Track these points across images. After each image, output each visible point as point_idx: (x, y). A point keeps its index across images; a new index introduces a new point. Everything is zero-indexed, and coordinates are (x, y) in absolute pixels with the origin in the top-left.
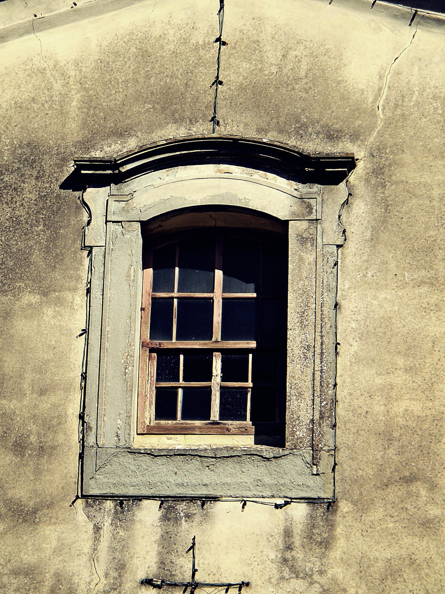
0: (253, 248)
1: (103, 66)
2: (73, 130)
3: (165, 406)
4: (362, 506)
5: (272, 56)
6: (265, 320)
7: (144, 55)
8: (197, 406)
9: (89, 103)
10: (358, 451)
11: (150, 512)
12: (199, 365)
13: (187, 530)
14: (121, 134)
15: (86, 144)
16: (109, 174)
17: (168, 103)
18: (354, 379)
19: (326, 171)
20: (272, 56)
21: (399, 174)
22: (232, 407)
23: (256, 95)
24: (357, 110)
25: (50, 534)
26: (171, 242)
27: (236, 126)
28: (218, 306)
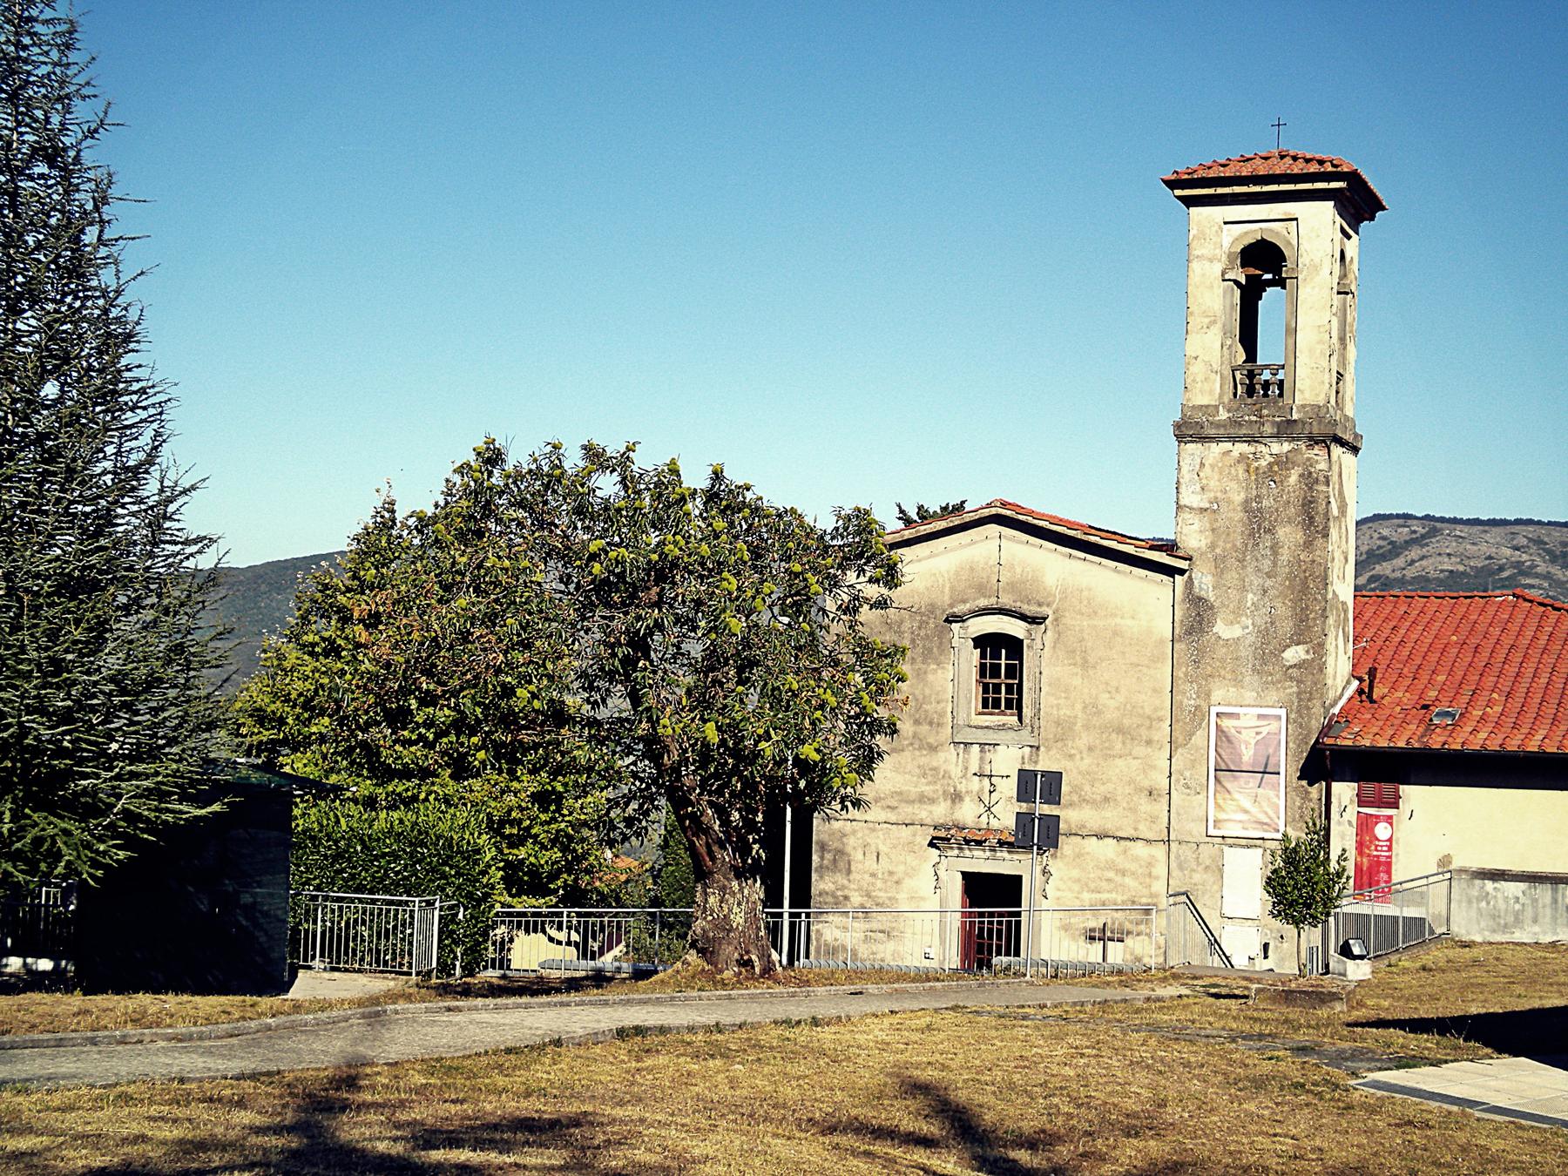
0: (1014, 646)
1: (957, 573)
2: (947, 600)
3: (985, 706)
4: (1048, 749)
5: (1019, 570)
6: (1015, 671)
7: (972, 569)
8: (996, 704)
9: (952, 589)
10: (1048, 729)
11: (976, 748)
12: (997, 688)
13: (988, 756)
14: (964, 602)
15: (951, 606)
16: (960, 619)
17: (981, 589)
18: (1046, 700)
19: (1034, 620)
20: (1019, 570)
21: (1064, 621)
22: (1009, 705)
23: (1013, 587)
24: (1049, 594)
25: (942, 755)
26: (981, 642)
27: (1006, 601)
28: (628, 1014)
